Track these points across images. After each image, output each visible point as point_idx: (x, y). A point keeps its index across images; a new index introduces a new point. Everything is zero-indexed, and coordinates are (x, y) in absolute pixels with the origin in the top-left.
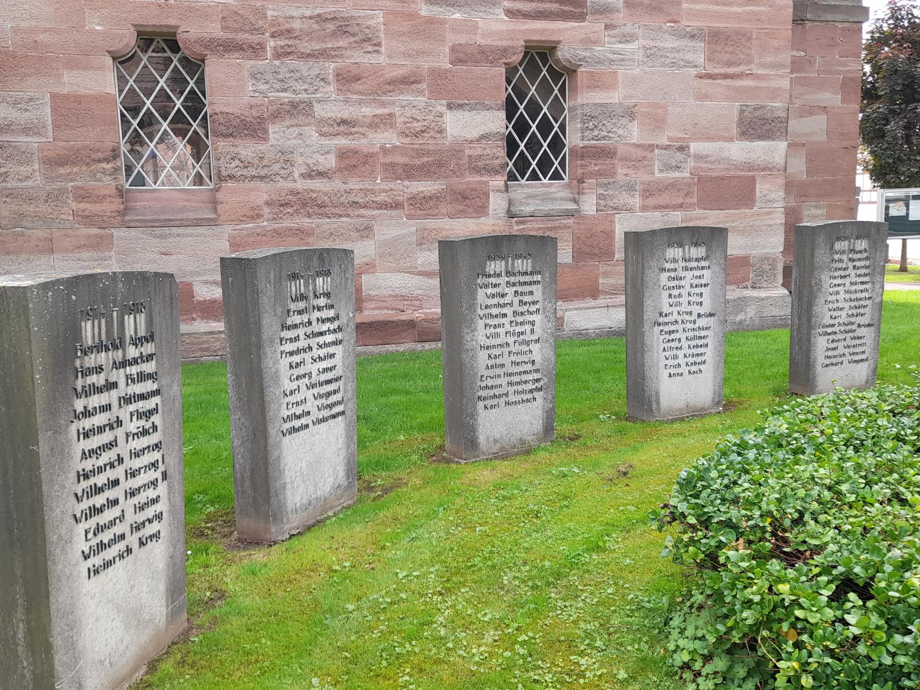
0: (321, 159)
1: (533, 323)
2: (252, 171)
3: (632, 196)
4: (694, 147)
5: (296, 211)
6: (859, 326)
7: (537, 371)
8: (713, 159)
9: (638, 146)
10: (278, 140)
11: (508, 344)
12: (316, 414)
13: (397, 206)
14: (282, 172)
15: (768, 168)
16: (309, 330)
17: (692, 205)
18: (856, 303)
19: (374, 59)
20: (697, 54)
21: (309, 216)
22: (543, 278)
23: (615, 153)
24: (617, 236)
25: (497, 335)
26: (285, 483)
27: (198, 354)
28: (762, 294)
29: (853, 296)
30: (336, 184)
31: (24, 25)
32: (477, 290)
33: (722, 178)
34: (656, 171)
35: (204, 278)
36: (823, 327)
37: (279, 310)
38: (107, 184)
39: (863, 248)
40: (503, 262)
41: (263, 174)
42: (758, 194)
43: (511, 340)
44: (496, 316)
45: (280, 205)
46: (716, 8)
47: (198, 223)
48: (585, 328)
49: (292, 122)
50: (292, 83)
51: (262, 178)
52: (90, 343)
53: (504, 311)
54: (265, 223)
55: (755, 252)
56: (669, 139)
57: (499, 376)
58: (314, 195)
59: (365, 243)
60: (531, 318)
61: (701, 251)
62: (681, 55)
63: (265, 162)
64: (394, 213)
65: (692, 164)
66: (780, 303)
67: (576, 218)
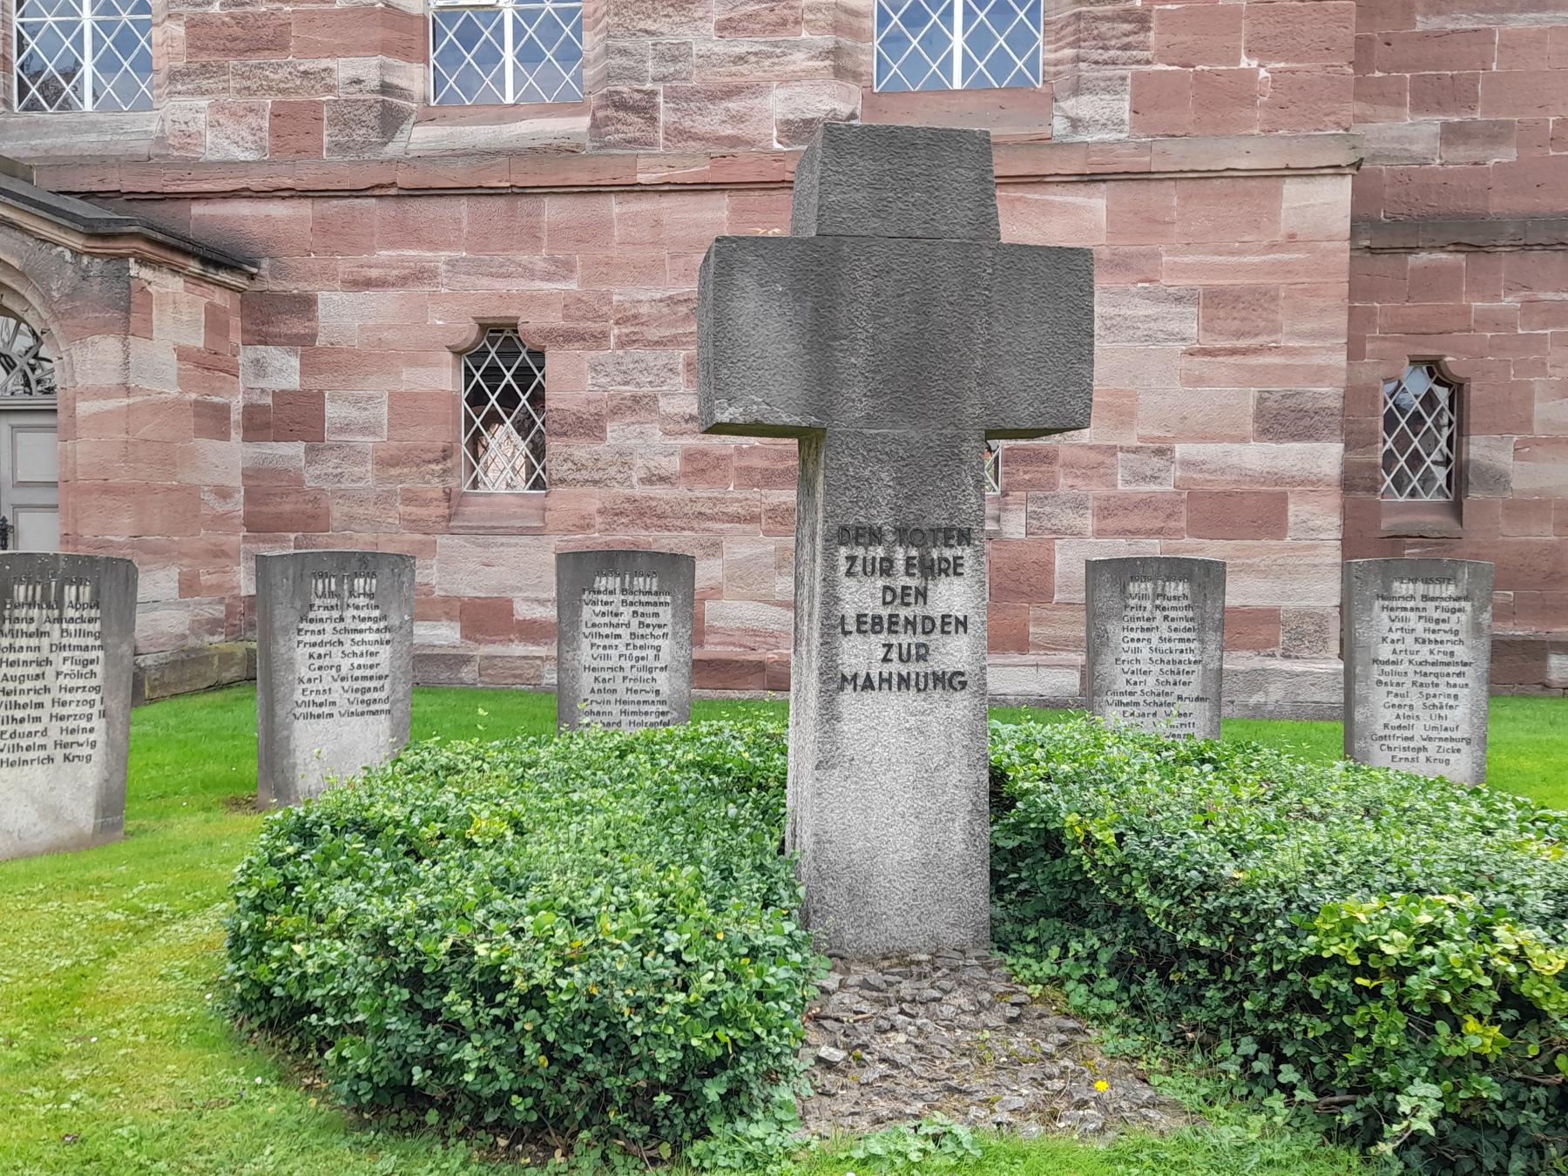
0: (664, 462)
1: (658, 649)
2: (585, 475)
3: (1081, 516)
4: (1180, 450)
5: (632, 522)
6: (1180, 698)
7: (663, 702)
8: (1213, 467)
9: (1091, 448)
10: (616, 439)
11: (621, 668)
12: (342, 704)
13: (753, 519)
14: (618, 476)
15: (1309, 484)
16: (340, 626)
17: (1178, 531)
18: (1174, 668)
20: (1187, 322)
21: (647, 528)
22: (674, 600)
23: (1056, 457)
24: (1057, 569)
25: (608, 657)
26: (295, 764)
27: (510, 681)
28: (1298, 667)
29: (1167, 657)
30: (679, 492)
31: (370, 323)
32: (581, 607)
33: (1229, 495)
34: (1120, 482)
35: (526, 594)
36: (1114, 693)
37: (298, 604)
38: (435, 487)
39: (1180, 593)
40: (618, 579)
41: (597, 477)
42: (1291, 519)
43: (627, 664)
44: (607, 636)
45: (614, 513)
46: (1217, 259)
47: (524, 531)
48: (1001, 691)
49: (633, 419)
50: (636, 374)
51: (595, 482)
52: (22, 599)
53: (618, 631)
54: (597, 535)
55: (1288, 603)
56: (1140, 438)
57: (609, 702)
58: (654, 504)
59: (712, 562)
60: (656, 643)
62: (1160, 325)
63: (600, 465)
64: (748, 527)
65: (1178, 474)
66: (1330, 684)
67: (995, 543)
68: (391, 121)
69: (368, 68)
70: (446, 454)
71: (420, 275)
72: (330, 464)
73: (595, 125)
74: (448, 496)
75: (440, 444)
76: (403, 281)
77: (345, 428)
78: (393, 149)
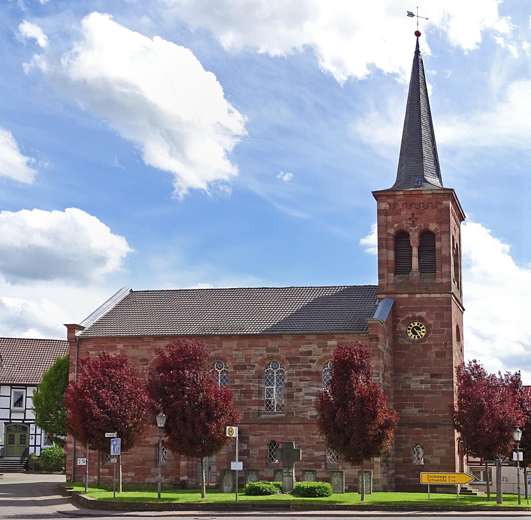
19: (303, 444)
61: (311, 473)
68: (259, 414)
69: (256, 408)
70: (266, 457)
71: (263, 434)
72: (251, 459)
73: (286, 415)
74: (266, 463)
75: (265, 456)
76: (260, 435)
77: (253, 454)
78: (259, 418)
